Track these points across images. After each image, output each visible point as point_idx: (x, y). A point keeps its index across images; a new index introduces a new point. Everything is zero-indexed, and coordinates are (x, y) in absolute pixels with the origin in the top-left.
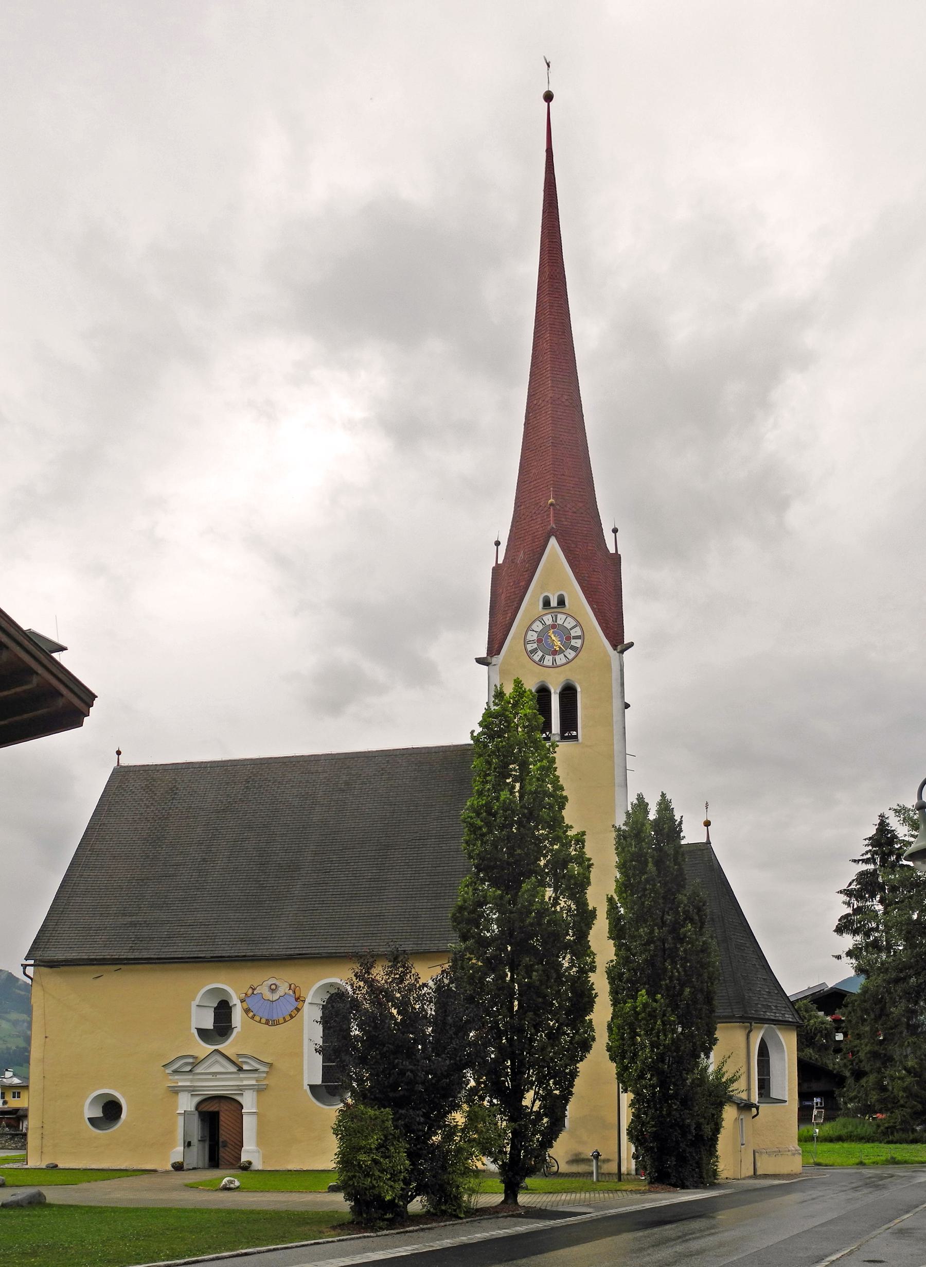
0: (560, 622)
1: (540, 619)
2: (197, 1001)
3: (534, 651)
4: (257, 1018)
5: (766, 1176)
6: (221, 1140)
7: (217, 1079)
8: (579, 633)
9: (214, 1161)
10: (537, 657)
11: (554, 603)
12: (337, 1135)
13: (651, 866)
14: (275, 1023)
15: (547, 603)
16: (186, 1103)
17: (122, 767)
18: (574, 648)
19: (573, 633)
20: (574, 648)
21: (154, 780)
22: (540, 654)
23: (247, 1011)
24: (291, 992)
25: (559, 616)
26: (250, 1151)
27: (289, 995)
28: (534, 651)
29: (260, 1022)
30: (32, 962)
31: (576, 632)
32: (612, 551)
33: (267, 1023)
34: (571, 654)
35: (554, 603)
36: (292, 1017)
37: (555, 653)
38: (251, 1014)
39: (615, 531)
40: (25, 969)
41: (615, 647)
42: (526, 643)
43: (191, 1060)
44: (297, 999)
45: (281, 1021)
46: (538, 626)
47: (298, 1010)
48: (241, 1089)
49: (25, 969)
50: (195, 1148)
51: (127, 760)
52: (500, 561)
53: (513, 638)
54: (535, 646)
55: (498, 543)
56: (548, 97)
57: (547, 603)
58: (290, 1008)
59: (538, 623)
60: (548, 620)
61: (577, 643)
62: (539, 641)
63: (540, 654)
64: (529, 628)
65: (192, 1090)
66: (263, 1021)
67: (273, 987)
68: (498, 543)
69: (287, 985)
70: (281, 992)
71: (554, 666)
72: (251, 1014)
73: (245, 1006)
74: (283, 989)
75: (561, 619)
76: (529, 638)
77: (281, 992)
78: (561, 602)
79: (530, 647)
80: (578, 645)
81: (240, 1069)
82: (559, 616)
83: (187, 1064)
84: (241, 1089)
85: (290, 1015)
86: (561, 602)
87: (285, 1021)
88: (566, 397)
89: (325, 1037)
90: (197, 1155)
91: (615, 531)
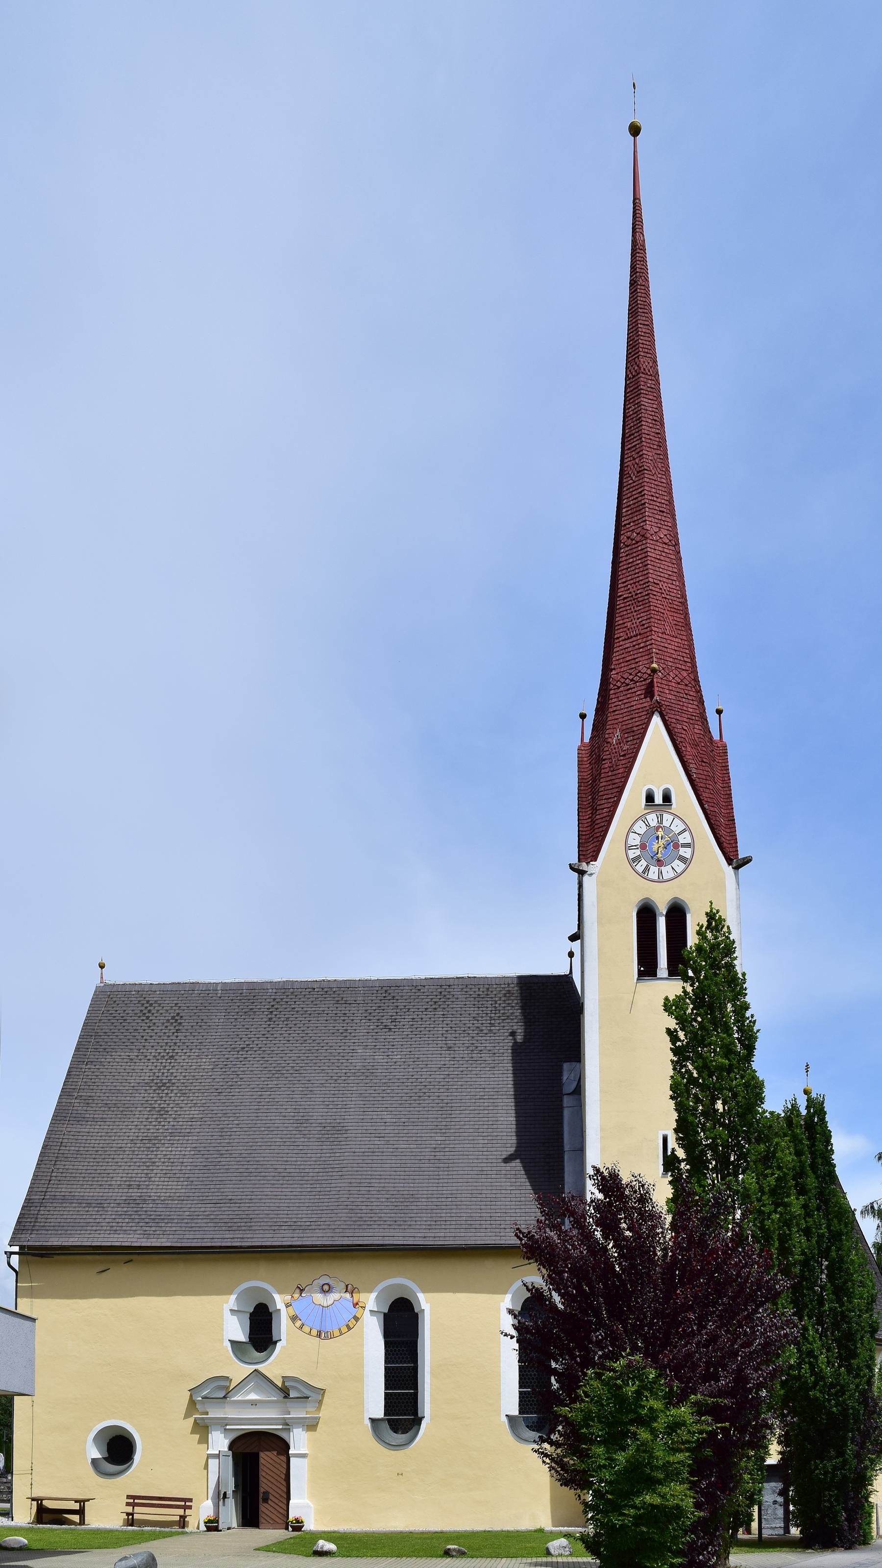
0: (666, 823)
3: (637, 859)
4: (306, 1329)
6: (262, 1490)
7: (256, 1412)
8: (688, 840)
9: (250, 1517)
10: (640, 868)
11: (658, 800)
14: (329, 1336)
15: (650, 798)
16: (220, 1442)
17: (106, 985)
18: (682, 859)
20: (682, 859)
21: (151, 1005)
22: (643, 863)
23: (294, 1319)
26: (303, 1504)
27: (346, 1299)
28: (637, 859)
29: (310, 1334)
30: (16, 1249)
31: (685, 838)
32: (716, 737)
33: (319, 1335)
34: (679, 866)
35: (658, 800)
36: (349, 1328)
37: (660, 863)
38: (298, 1324)
39: (719, 712)
40: (9, 1258)
41: (729, 861)
42: (628, 848)
44: (355, 1305)
45: (337, 1333)
46: (641, 828)
47: (356, 1319)
48: (288, 1425)
49: (9, 1258)
50: (231, 1502)
51: (116, 976)
52: (587, 740)
53: (612, 841)
54: (638, 852)
55: (583, 716)
56: (635, 130)
57: (650, 798)
59: (640, 823)
61: (686, 852)
62: (643, 846)
63: (643, 863)
65: (222, 1424)
66: (314, 1332)
67: (326, 1288)
68: (583, 716)
71: (660, 880)
72: (298, 1324)
73: (292, 1313)
75: (667, 818)
76: (631, 842)
78: (667, 798)
79: (632, 854)
80: (688, 855)
82: (666, 816)
85: (348, 1326)
86: (667, 798)
87: (341, 1334)
88: (666, 532)
90: (230, 1514)
91: (719, 712)
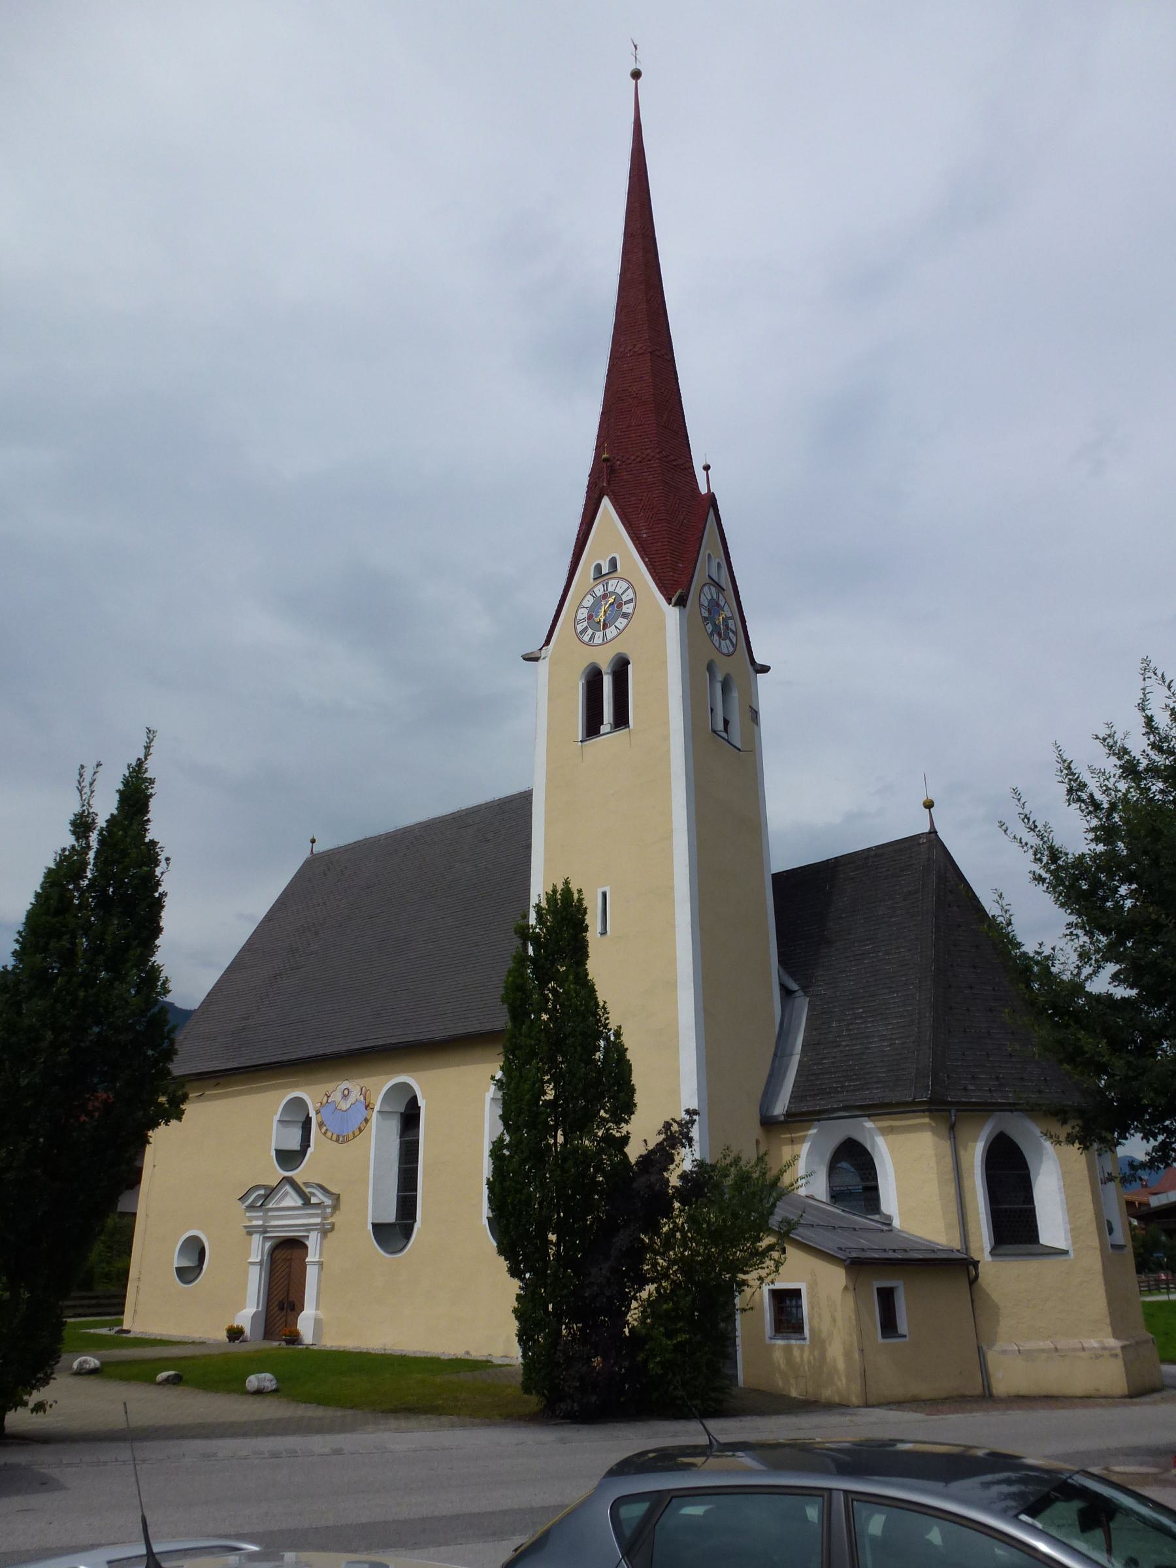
1: (591, 592)
2: (277, 1117)
3: (584, 630)
4: (329, 1134)
5: (364, 1562)
7: (288, 1215)
11: (605, 570)
12: (1140, 1204)
13: (579, 1049)
14: (346, 1140)
19: (599, 634)
22: (590, 631)
24: (362, 1098)
25: (611, 582)
33: (337, 1140)
36: (361, 1131)
42: (576, 623)
43: (262, 1192)
58: (361, 1119)
60: (599, 591)
61: (627, 609)
64: (580, 606)
66: (334, 1137)
69: (358, 1088)
70: (352, 1099)
74: (355, 1095)
77: (352, 1099)
81: (307, 1202)
82: (611, 582)
83: (259, 1196)
84: (308, 1228)
86: (613, 563)
89: (10, 1410)
